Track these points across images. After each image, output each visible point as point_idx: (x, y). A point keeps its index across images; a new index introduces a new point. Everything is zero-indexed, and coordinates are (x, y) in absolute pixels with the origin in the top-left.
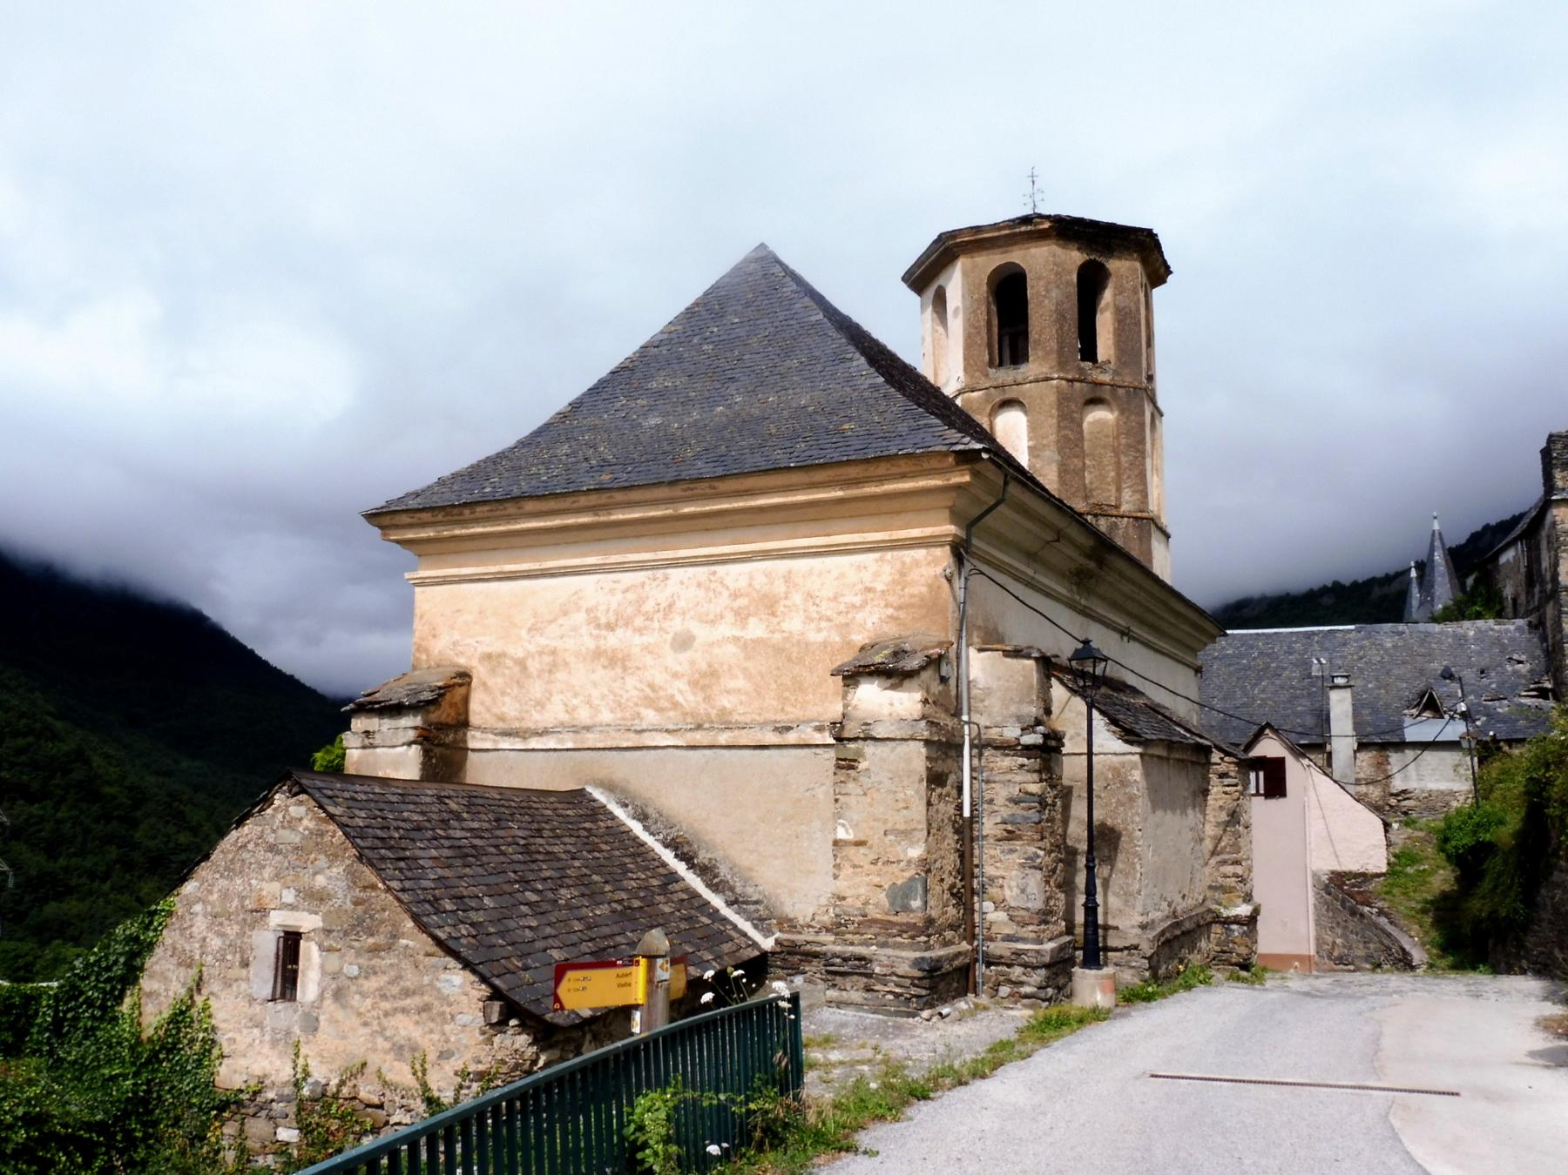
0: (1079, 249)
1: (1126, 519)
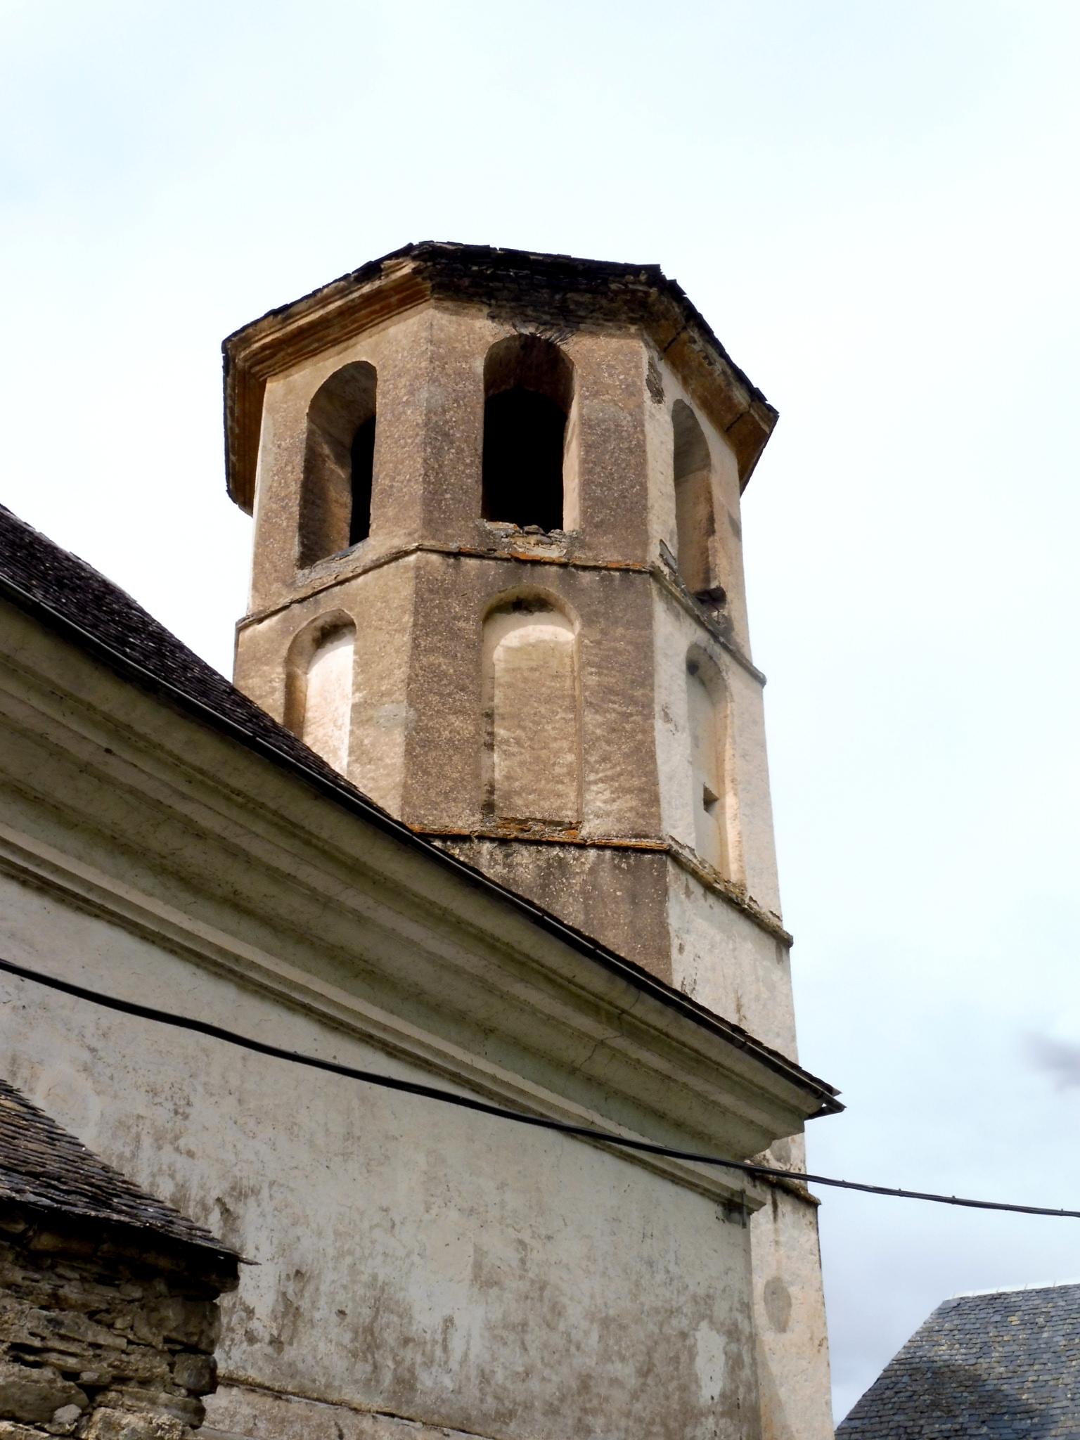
0: (492, 317)
1: (592, 853)
